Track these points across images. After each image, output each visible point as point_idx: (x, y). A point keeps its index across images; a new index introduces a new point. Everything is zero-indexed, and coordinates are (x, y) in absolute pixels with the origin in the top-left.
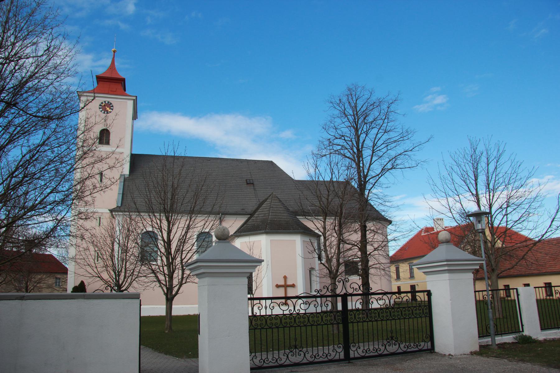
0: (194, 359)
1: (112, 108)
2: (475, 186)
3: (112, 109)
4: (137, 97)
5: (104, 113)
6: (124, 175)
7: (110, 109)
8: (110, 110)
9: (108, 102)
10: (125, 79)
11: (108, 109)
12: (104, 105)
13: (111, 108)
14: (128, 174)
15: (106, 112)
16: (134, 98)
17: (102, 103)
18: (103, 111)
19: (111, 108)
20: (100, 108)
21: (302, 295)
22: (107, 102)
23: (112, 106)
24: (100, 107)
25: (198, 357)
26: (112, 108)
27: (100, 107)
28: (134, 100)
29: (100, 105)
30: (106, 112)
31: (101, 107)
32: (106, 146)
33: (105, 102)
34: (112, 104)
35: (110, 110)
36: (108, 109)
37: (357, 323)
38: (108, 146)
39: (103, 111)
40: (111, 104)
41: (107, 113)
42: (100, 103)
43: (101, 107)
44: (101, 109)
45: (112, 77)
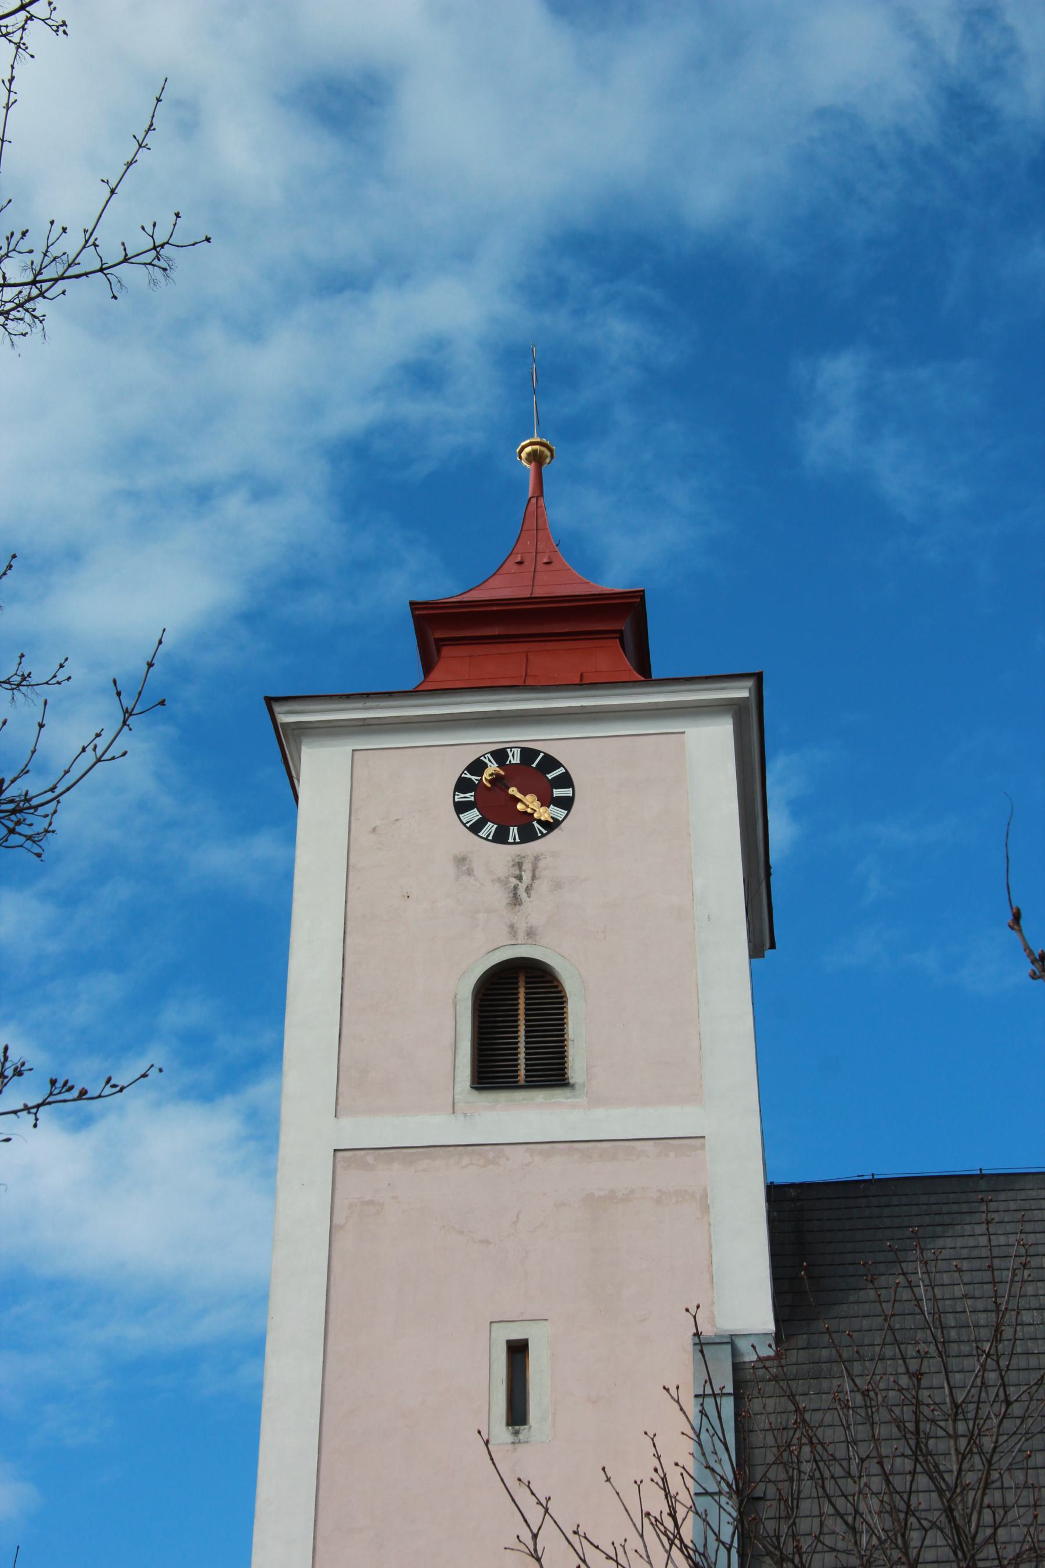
0: (781, 1179)
1: (567, 792)
2: (647, 1559)
3: (566, 803)
4: (758, 677)
5: (501, 838)
6: (731, 1341)
7: (547, 801)
8: (545, 813)
9: (529, 754)
10: (641, 595)
11: (529, 803)
12: (496, 780)
13: (557, 793)
14: (771, 1327)
15: (514, 831)
16: (741, 692)
17: (478, 767)
18: (490, 828)
19: (557, 793)
20: (461, 808)
21: (982, 1518)
22: (515, 758)
23: (566, 780)
24: (460, 797)
25: (775, 1194)
26: (567, 792)
27: (460, 797)
28: (737, 710)
29: (462, 785)
30: (514, 831)
31: (470, 797)
32: (539, 1096)
33: (500, 756)
34: (557, 764)
35: (545, 813)
36: (529, 803)
37: (993, 1524)
38: (558, 1095)
39: (490, 828)
40: (551, 763)
41: (528, 835)
42: (457, 766)
43: (470, 797)
44: (473, 815)
45: (540, 592)
